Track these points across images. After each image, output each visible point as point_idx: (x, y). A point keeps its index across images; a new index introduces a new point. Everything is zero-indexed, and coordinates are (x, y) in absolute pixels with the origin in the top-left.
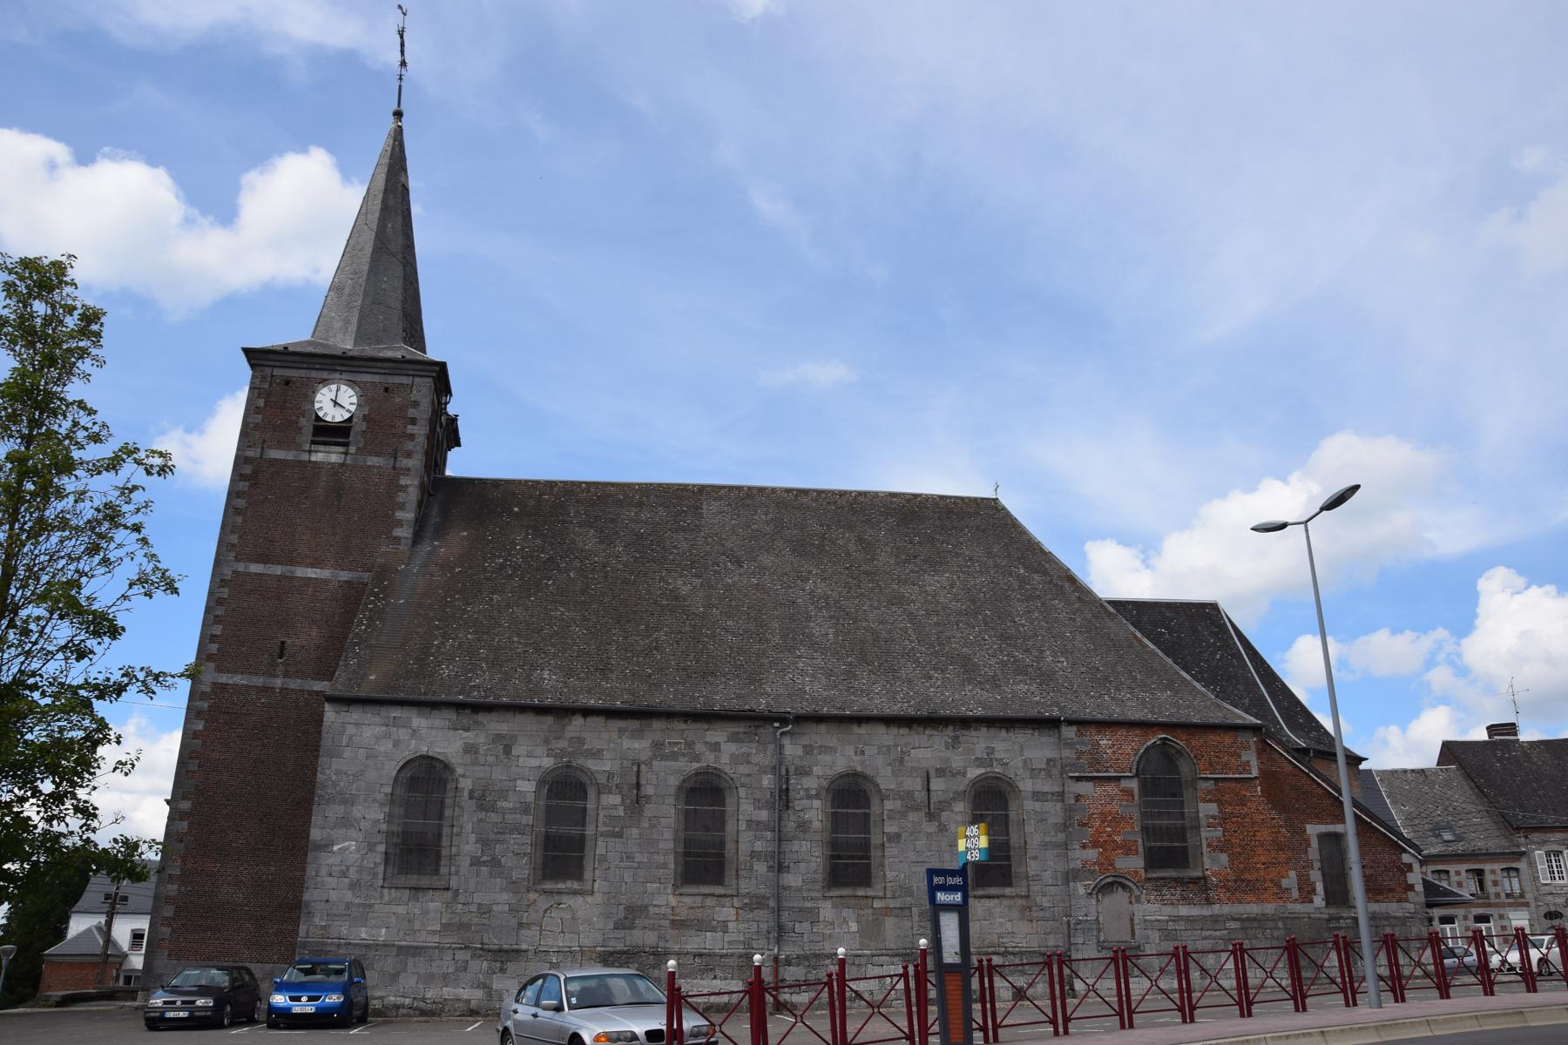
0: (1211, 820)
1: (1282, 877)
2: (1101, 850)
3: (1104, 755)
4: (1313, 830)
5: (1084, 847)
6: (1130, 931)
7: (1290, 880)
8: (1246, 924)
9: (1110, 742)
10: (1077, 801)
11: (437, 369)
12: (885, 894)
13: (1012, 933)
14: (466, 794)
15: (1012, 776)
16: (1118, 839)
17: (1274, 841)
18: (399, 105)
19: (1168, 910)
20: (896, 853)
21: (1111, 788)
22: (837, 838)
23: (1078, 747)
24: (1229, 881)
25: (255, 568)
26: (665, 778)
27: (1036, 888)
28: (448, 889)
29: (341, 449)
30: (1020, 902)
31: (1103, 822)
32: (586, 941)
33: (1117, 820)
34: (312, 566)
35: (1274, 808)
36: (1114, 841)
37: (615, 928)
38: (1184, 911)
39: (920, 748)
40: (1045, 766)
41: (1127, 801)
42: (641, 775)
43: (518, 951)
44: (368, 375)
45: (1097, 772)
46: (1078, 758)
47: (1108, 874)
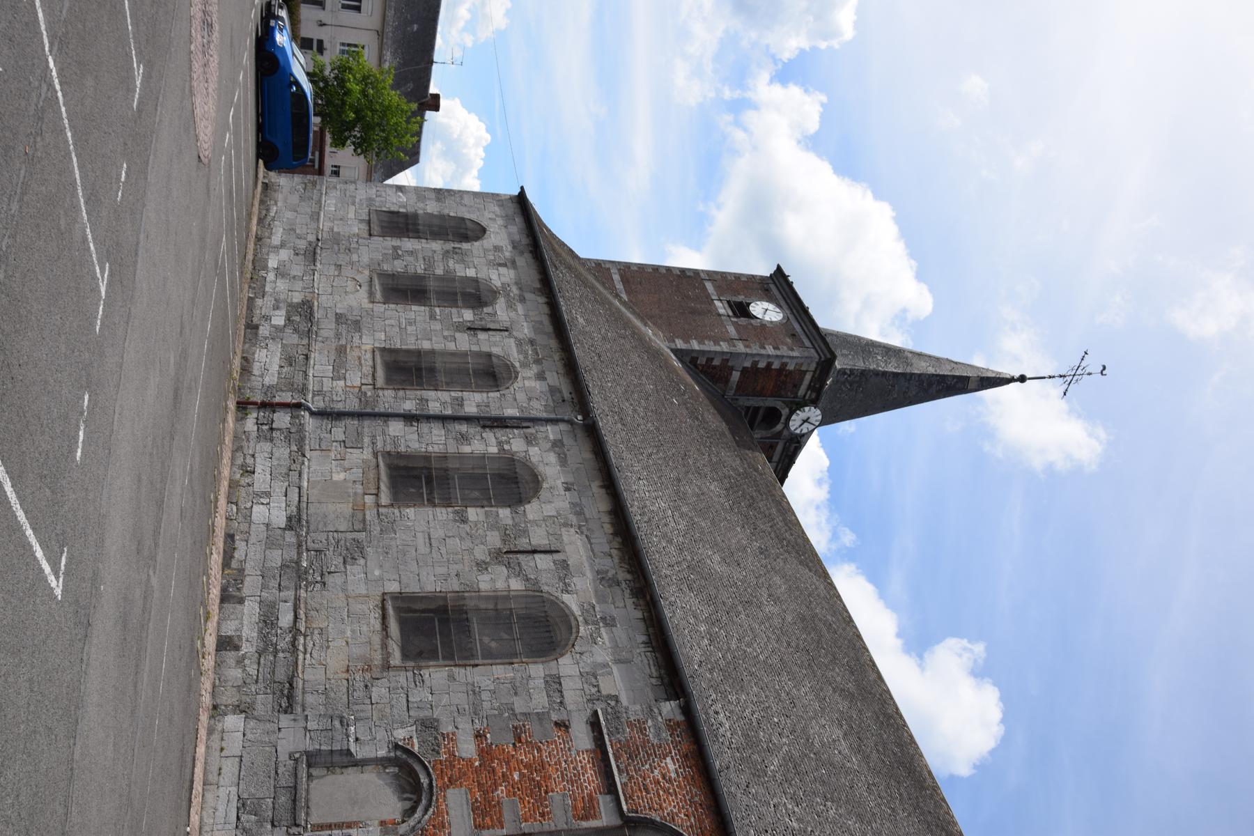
2: (477, 764)
3: (647, 766)
5: (479, 736)
6: (329, 821)
9: (673, 775)
10: (556, 724)
11: (829, 356)
12: (378, 389)
13: (328, 647)
14: (459, 246)
15: (577, 648)
16: (501, 791)
18: (1029, 379)
20: (440, 518)
21: (591, 781)
22: (456, 488)
23: (650, 723)
26: (503, 347)
27: (402, 680)
28: (370, 235)
29: (731, 313)
30: (377, 658)
36: (496, 786)
37: (336, 314)
39: (591, 544)
40: (604, 693)
41: (575, 808)
42: (498, 332)
43: (314, 261)
44: (780, 297)
45: (614, 754)
46: (630, 725)
47: (434, 777)
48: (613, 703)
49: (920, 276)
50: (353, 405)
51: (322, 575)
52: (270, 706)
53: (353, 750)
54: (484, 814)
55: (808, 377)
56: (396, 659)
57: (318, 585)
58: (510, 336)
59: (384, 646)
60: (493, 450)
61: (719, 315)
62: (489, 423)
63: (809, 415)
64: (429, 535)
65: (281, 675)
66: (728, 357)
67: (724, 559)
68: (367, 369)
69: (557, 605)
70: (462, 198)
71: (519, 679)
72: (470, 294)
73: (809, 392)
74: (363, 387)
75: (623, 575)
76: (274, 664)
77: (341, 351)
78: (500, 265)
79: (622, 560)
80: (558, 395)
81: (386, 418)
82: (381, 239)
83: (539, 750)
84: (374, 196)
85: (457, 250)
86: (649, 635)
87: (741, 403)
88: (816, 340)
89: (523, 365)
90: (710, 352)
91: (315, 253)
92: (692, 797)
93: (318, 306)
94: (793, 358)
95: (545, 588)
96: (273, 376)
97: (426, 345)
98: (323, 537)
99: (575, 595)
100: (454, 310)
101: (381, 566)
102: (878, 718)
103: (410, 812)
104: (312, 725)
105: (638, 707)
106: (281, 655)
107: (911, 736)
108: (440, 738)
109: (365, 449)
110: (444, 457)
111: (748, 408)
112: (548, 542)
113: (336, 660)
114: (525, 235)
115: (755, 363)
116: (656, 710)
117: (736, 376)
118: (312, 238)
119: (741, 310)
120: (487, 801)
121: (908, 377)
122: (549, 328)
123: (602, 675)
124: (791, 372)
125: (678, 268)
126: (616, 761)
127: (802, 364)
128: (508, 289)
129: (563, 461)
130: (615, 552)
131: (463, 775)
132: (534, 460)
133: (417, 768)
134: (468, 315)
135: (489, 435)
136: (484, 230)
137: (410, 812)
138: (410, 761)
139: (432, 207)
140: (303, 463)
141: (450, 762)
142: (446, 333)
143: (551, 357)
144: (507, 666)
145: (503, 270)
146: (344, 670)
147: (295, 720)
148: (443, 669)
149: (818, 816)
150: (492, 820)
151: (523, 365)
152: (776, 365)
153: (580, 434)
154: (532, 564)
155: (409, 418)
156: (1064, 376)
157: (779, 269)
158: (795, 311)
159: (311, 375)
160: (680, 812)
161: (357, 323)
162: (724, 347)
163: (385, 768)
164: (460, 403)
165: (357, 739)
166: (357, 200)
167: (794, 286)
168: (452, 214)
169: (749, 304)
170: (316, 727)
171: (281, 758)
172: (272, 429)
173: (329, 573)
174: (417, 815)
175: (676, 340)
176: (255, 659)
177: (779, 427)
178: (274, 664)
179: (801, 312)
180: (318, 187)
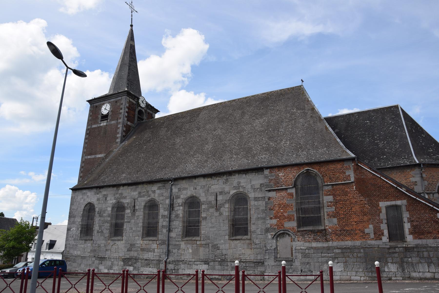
0: (329, 204)
1: (365, 228)
2: (278, 219)
3: (281, 180)
4: (383, 204)
5: (271, 218)
7: (370, 229)
8: (344, 251)
9: (283, 174)
10: (269, 200)
11: (126, 92)
13: (244, 254)
14: (97, 212)
16: (286, 214)
17: (361, 211)
18: (132, 23)
19: (307, 244)
20: (205, 224)
21: (283, 193)
23: (270, 178)
24: (337, 231)
25: (89, 157)
26: (141, 203)
27: (254, 236)
28: (92, 240)
29: (106, 121)
30: (248, 241)
31: (279, 208)
32: (121, 255)
33: (285, 206)
34: (100, 154)
35: (362, 195)
36: (284, 215)
37: (127, 251)
38: (314, 245)
39: (214, 185)
40: (259, 187)
41: (290, 198)
42: (135, 203)
43: (105, 258)
45: (277, 187)
46: (270, 182)
47: (281, 229)
48: (262, 185)
49: (28, 21)
50: (165, 247)
51: (223, 255)
52: (261, 267)
53: (274, 248)
54: (291, 219)
55: (131, 100)
56: (248, 237)
57: (226, 256)
58: (137, 199)
59: (244, 240)
60: (181, 208)
61: (107, 125)
62: (171, 208)
63: (141, 101)
64: (211, 227)
65: (253, 265)
66: (123, 125)
67: (206, 144)
68: (151, 242)
69: (233, 196)
70: (73, 209)
71: (255, 207)
72: (117, 210)
73: (135, 100)
74: (157, 243)
75: (225, 177)
76: (249, 267)
77: (143, 250)
78: (106, 199)
79: (220, 177)
80: (161, 187)
81: (169, 237)
82: (93, 237)
83: (275, 205)
84: (73, 238)
85: (99, 212)
86: (243, 174)
87: (136, 122)
88: (120, 95)
89: (149, 196)
90: (122, 131)
91: (101, 258)
92: (289, 171)
93: (124, 257)
94: (125, 104)
95: (228, 198)
96: (154, 269)
97: (141, 224)
98: (211, 255)
99: (231, 191)
100: (126, 215)
101: (220, 240)
102: (248, 106)
103: (289, 235)
104: (267, 257)
105: (265, 180)
106: (247, 265)
107: (252, 96)
108: (271, 228)
109: (181, 243)
110: (184, 222)
111: (138, 120)
112: (214, 196)
113: (248, 252)
114: (92, 190)
115: (126, 117)
116: (266, 176)
117: (129, 123)
118: (94, 259)
119: (105, 117)
120: (288, 218)
121: (130, 65)
122: (134, 187)
123: (254, 187)
124: (129, 105)
125: (85, 136)
126: (279, 187)
127: (127, 102)
128: (117, 198)
129: (186, 189)
130: (217, 179)
131: (281, 223)
132: (185, 197)
133: (279, 233)
134: (128, 211)
135: (176, 209)
136: (90, 203)
137: (289, 235)
138: (277, 235)
139: (78, 220)
140: (186, 261)
141: (278, 225)
142: (136, 218)
143: (146, 188)
144: (251, 210)
145: (108, 199)
146: (251, 250)
147: (266, 261)
148: (251, 226)
149: (284, 135)
150: (292, 217)
151: (149, 196)
152: (127, 110)
153: (176, 183)
154: (220, 201)
155: (169, 231)
156: (132, 11)
157: (88, 101)
158: (106, 99)
159: (153, 259)
160: (293, 174)
161: (131, 245)
162: (120, 126)
163: (278, 240)
164: (163, 216)
165: (271, 247)
166: (75, 244)
167: (96, 97)
168: (82, 213)
169: (102, 114)
170: (268, 256)
171: (276, 264)
172: (174, 269)
173: (222, 253)
174: (290, 234)
175: (117, 141)
176: (248, 271)
177: (143, 110)
178: (249, 267)
179: (107, 97)
180: (69, 257)
